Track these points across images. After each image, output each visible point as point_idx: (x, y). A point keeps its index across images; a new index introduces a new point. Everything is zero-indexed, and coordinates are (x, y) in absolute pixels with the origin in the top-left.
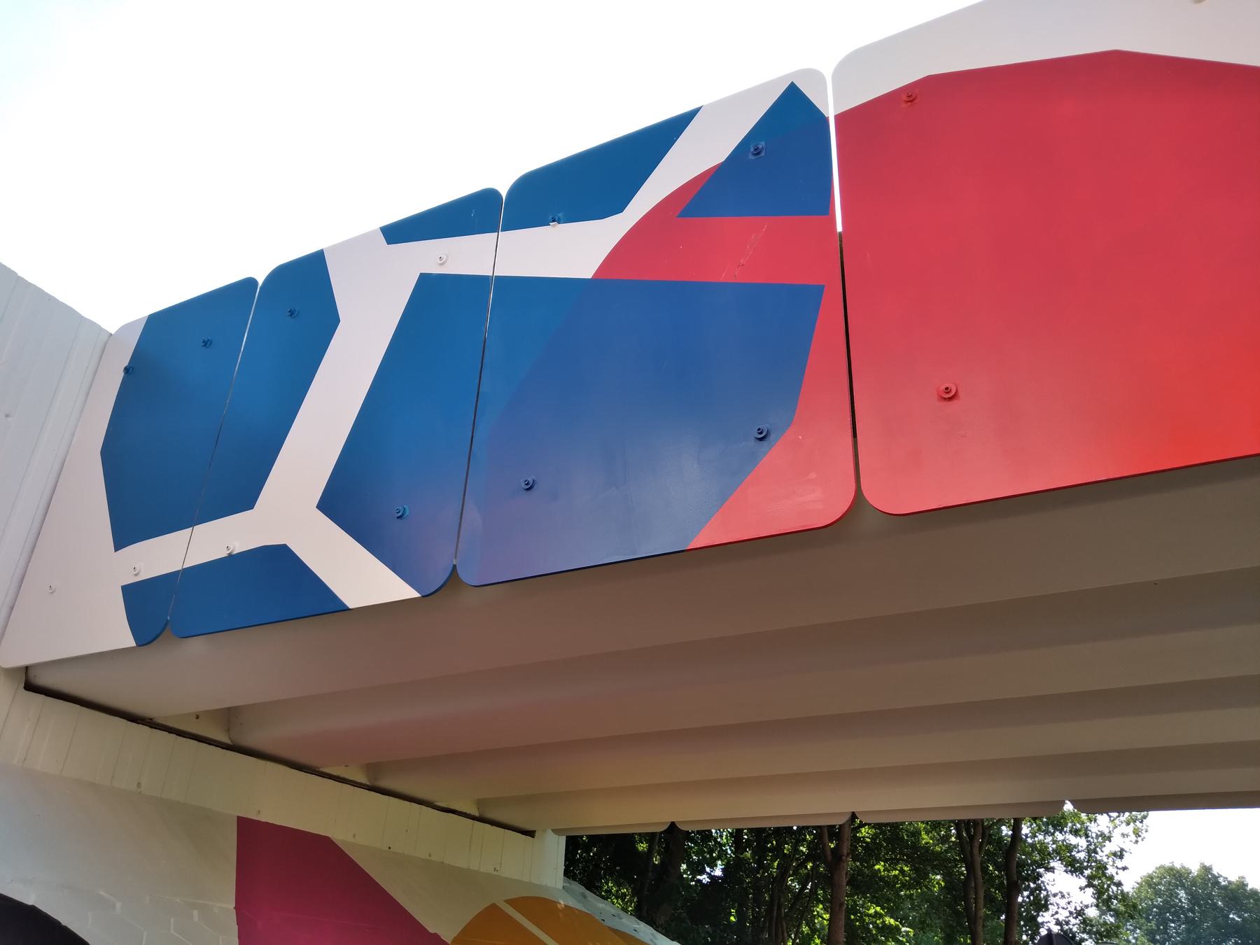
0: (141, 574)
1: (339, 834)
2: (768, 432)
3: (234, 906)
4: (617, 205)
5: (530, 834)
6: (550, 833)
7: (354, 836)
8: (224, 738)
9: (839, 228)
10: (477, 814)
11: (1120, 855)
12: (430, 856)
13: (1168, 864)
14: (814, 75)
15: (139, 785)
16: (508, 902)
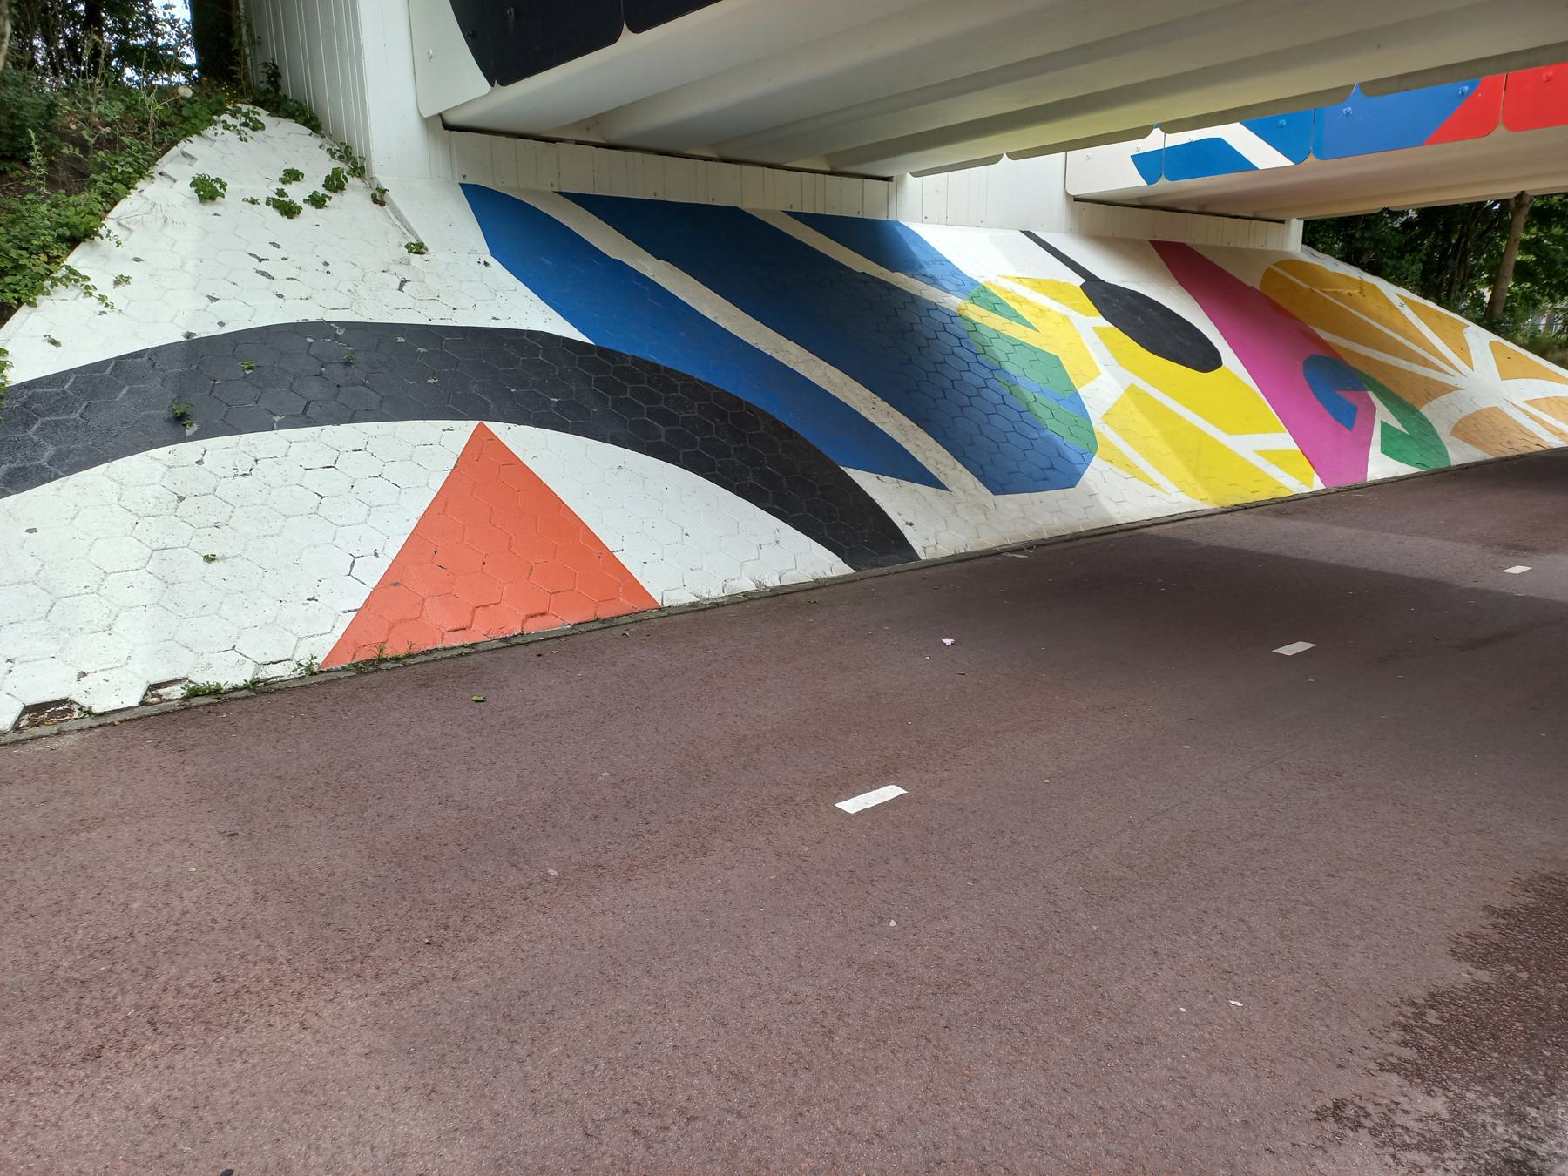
5: (1282, 222)
10: (827, 168)
16: (1275, 265)
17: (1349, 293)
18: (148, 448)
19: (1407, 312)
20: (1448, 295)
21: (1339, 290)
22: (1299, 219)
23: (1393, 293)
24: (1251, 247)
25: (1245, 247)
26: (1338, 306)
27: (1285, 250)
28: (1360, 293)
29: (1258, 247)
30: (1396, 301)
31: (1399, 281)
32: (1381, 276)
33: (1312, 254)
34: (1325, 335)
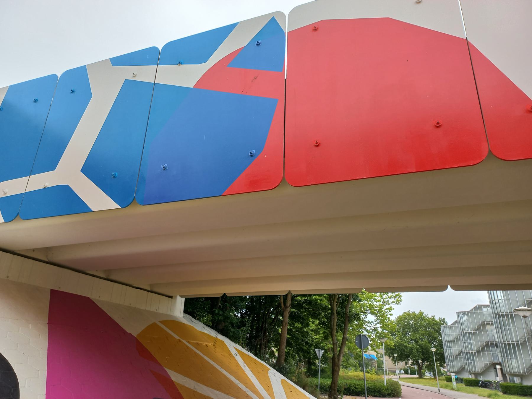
0: (7, 193)
1: (94, 296)
2: (319, 144)
3: (47, 322)
4: (204, 59)
5: (171, 297)
6: (179, 296)
7: (99, 297)
8: (46, 260)
9: (285, 78)
10: (149, 289)
11: (390, 309)
12: (130, 304)
13: (406, 311)
14: (281, 14)
15: (8, 277)
16: (160, 322)
17: (206, 345)
18: (272, 367)
19: (239, 359)
20: (260, 351)
21: (200, 342)
22: (181, 296)
23: (232, 346)
24: (148, 309)
25: (143, 308)
26: (195, 353)
27: (172, 314)
28: (214, 345)
29: (153, 309)
30: (233, 352)
31: (234, 338)
32: (227, 337)
33: (192, 320)
34: (176, 377)
